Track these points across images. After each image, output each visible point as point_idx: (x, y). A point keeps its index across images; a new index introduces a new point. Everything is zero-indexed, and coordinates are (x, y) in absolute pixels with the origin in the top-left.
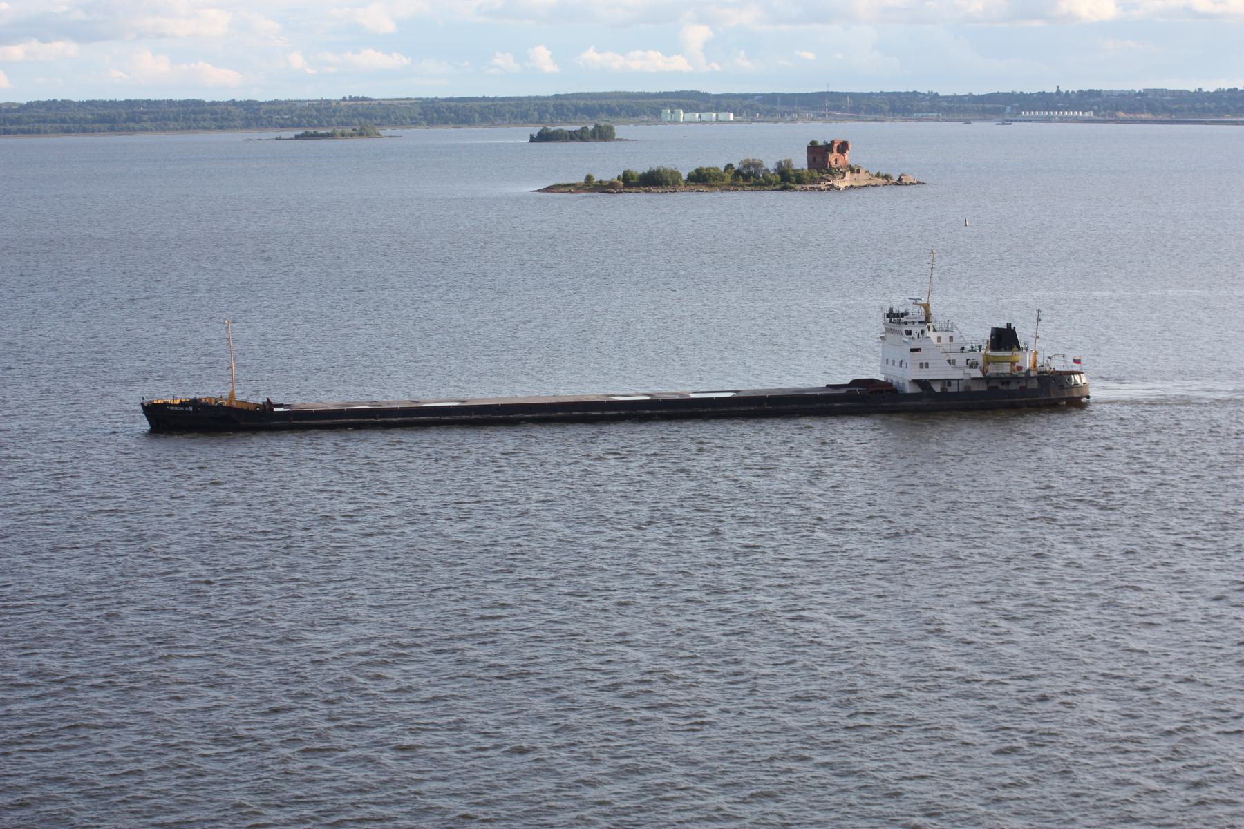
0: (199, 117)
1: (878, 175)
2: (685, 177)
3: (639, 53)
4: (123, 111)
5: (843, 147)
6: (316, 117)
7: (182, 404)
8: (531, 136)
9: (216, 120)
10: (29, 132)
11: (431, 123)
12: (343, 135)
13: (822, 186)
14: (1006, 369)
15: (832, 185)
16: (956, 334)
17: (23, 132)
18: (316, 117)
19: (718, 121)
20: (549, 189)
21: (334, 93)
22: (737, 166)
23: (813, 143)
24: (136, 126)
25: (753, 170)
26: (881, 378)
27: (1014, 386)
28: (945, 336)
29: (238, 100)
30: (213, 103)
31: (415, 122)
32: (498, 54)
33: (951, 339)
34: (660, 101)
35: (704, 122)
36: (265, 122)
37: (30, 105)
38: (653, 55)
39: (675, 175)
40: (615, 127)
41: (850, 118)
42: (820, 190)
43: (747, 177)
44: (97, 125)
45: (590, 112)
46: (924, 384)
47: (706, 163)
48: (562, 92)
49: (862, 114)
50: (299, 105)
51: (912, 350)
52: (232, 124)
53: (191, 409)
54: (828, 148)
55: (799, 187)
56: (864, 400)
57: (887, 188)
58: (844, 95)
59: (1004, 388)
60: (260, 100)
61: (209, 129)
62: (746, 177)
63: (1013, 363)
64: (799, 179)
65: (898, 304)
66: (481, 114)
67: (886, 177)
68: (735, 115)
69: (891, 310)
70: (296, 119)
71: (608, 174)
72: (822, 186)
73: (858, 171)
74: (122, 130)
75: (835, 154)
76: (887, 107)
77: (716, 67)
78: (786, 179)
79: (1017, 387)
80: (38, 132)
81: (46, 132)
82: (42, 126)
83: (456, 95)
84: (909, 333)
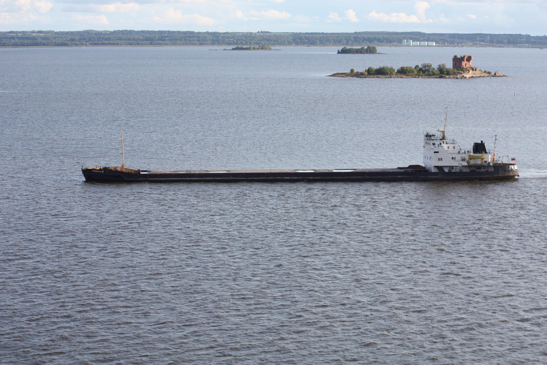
0: (192, 39)
1: (485, 72)
2: (396, 71)
3: (395, 14)
4: (157, 35)
5: (469, 59)
6: (245, 40)
7: (100, 169)
8: (338, 51)
9: (199, 40)
10: (113, 44)
11: (297, 44)
12: (254, 49)
13: (458, 76)
14: (479, 162)
15: (463, 76)
16: (456, 146)
17: (111, 44)
18: (245, 40)
19: (428, 46)
20: (334, 75)
21: (254, 29)
22: (420, 66)
23: (455, 56)
24: (162, 42)
25: (427, 68)
26: (423, 165)
27: (483, 170)
28: (451, 146)
29: (210, 31)
30: (199, 33)
31: (289, 43)
33: (454, 147)
35: (421, 46)
36: (221, 42)
37: (115, 32)
38: (402, 15)
39: (392, 70)
42: (457, 78)
43: (424, 72)
44: (145, 42)
45: (370, 40)
46: (440, 168)
47: (406, 64)
48: (358, 31)
49: (494, 44)
50: (237, 34)
51: (435, 152)
52: (206, 42)
53: (103, 172)
54: (462, 59)
55: (447, 76)
56: (414, 175)
57: (488, 78)
58: (487, 35)
59: (478, 170)
60: (220, 32)
61: (196, 44)
62: (424, 72)
63: (482, 159)
64: (448, 73)
66: (320, 40)
67: (489, 73)
68: (436, 43)
70: (235, 41)
71: (361, 69)
72: (458, 76)
73: (476, 70)
74: (156, 44)
75: (465, 62)
76: (506, 41)
78: (442, 73)
79: (484, 170)
80: (118, 44)
81: (121, 44)
82: (119, 42)
83: (310, 31)
84: (434, 144)
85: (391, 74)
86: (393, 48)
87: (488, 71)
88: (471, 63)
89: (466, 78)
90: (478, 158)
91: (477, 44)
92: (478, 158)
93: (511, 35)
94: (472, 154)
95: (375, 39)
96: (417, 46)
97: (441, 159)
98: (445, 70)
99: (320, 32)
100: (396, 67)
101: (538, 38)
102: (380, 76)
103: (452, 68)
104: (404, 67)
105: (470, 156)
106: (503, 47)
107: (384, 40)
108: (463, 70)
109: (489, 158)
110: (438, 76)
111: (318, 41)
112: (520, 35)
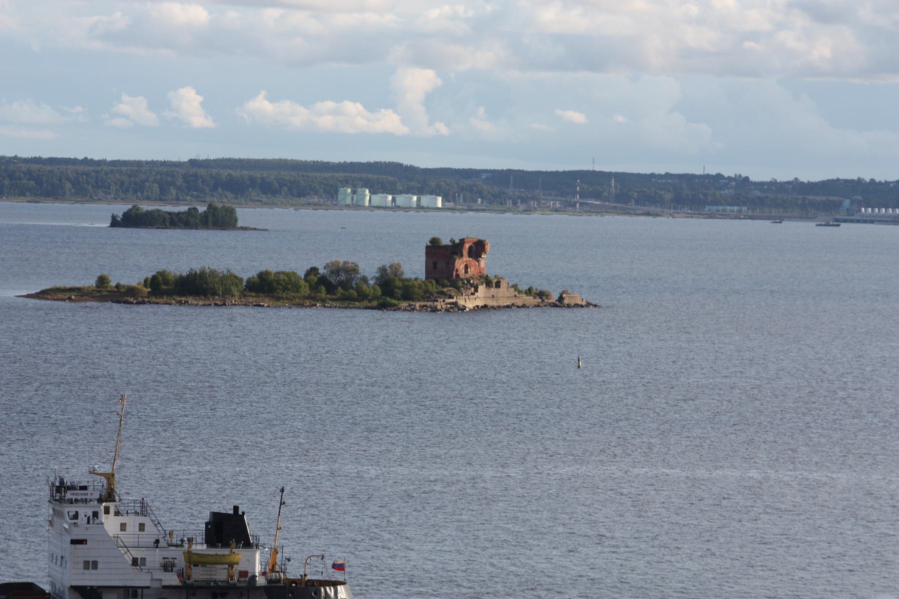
1: (529, 292)
3: (330, 104)
5: (478, 248)
8: (114, 218)
14: (221, 575)
15: (456, 304)
19: (420, 208)
20: (42, 295)
23: (434, 242)
25: (343, 277)
28: (133, 522)
32: (125, 97)
33: (142, 527)
34: (341, 175)
35: (399, 208)
38: (353, 108)
42: (434, 310)
43: (334, 288)
47: (273, 266)
49: (632, 205)
51: (74, 542)
54: (456, 249)
55: (404, 304)
57: (534, 313)
58: (609, 175)
62: (331, 289)
65: (76, 474)
67: (541, 295)
68: (445, 199)
69: (62, 481)
71: (133, 277)
72: (440, 304)
73: (498, 285)
75: (466, 258)
76: (669, 196)
77: (442, 128)
78: (390, 292)
85: (227, 292)
87: (538, 286)
88: (483, 263)
89: (464, 308)
90: (216, 561)
91: (574, 205)
92: (216, 561)
94: (200, 547)
95: (253, 181)
96: (386, 208)
97: (95, 565)
98: (398, 283)
100: (247, 271)
101: (774, 186)
102: (191, 300)
103: (422, 276)
104: (267, 273)
105: (189, 555)
106: (656, 215)
109: (256, 563)
110: (375, 303)
111: (68, 185)
112: (719, 176)
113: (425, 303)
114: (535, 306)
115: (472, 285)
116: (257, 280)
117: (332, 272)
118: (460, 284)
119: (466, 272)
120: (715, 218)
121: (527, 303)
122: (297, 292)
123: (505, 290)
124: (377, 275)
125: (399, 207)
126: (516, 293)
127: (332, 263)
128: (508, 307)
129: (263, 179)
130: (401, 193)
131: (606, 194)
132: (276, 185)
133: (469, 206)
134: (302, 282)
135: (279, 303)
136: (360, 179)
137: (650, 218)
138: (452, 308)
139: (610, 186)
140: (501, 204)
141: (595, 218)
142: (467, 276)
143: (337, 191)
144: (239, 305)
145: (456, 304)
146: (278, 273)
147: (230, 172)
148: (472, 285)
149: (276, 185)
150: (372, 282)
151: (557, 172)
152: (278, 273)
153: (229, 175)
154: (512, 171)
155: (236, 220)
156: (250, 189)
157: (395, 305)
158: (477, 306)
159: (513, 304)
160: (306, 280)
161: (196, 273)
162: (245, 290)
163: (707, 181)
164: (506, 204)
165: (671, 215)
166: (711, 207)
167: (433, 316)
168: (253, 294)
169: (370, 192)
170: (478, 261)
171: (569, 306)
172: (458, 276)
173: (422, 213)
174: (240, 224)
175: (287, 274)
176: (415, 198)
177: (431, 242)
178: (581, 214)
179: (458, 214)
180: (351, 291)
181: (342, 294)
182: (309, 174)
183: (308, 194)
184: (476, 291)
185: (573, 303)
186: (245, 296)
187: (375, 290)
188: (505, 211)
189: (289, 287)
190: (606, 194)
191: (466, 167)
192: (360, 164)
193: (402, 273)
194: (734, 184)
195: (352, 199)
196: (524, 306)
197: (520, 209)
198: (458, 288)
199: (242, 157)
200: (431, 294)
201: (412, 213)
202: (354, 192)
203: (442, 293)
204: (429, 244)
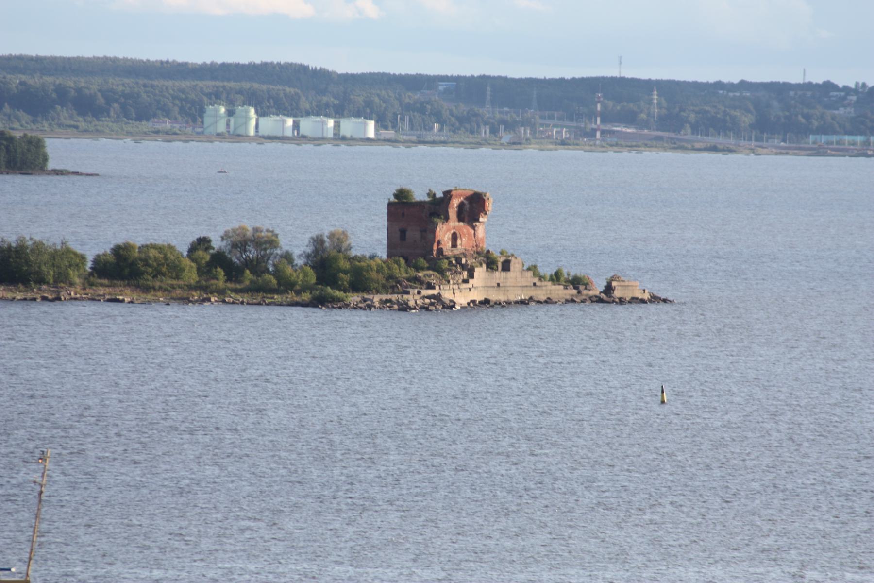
1: (556, 278)
5: (473, 207)
15: (438, 297)
19: (339, 138)
23: (402, 195)
25: (252, 253)
34: (208, 84)
40: (46, 140)
41: (655, 143)
42: (404, 308)
43: (238, 271)
47: (138, 235)
49: (687, 134)
54: (437, 207)
55: (354, 298)
58: (648, 85)
62: (233, 272)
67: (576, 282)
68: (381, 124)
72: (412, 298)
76: (747, 119)
78: (331, 279)
85: (62, 279)
86: (153, 146)
87: (571, 270)
88: (481, 230)
89: (451, 306)
91: (592, 134)
93: (779, 89)
96: (283, 139)
98: (344, 264)
99: (736, 81)
100: (94, 245)
104: (127, 247)
107: (109, 101)
108: (440, 265)
110: (306, 297)
112: (828, 86)
113: (389, 297)
114: (567, 301)
115: (464, 267)
116: (111, 259)
117: (234, 246)
118: (445, 264)
119: (454, 245)
120: (825, 154)
121: (554, 297)
122: (177, 278)
123: (518, 274)
124: (309, 250)
125: (304, 137)
126: (536, 280)
127: (234, 231)
128: (522, 302)
129: (79, 90)
130: (308, 114)
131: (643, 116)
132: (101, 101)
133: (419, 136)
134: (187, 263)
135: (149, 297)
136: (240, 92)
137: (719, 155)
138: (432, 304)
139: (650, 102)
140: (472, 132)
141: (626, 155)
142: (456, 252)
143: (202, 111)
144: (82, 299)
145: (438, 297)
146: (145, 248)
147: (24, 78)
148: (464, 267)
149: (101, 101)
150: (299, 262)
151: (562, 80)
152: (146, 247)
153: (21, 83)
154: (489, 77)
155: (45, 159)
156: (59, 107)
157: (339, 300)
158: (474, 301)
159: (531, 298)
160: (189, 256)
161: (10, 247)
162: (91, 274)
163: (809, 94)
164: (479, 133)
165: (752, 150)
166: (818, 137)
167: (404, 317)
168: (106, 282)
169: (257, 112)
170: (474, 228)
171: (621, 301)
172: (440, 251)
173: (343, 147)
174: (51, 165)
175: (160, 249)
176: (331, 123)
177: (396, 196)
178: (603, 148)
179: (402, 149)
180: (267, 276)
181: (252, 281)
182: (155, 83)
183: (155, 115)
184: (471, 275)
185: (628, 296)
186: (92, 284)
187: (306, 275)
188: (479, 144)
189: (164, 269)
190: (643, 116)
191: (412, 71)
192: (238, 66)
193: (350, 248)
194: (854, 98)
195: (228, 125)
196: (548, 301)
197: (503, 141)
198: (441, 272)
199: (42, 53)
200: (399, 282)
201: (328, 147)
202: (230, 113)
203: (416, 280)
204: (392, 199)
